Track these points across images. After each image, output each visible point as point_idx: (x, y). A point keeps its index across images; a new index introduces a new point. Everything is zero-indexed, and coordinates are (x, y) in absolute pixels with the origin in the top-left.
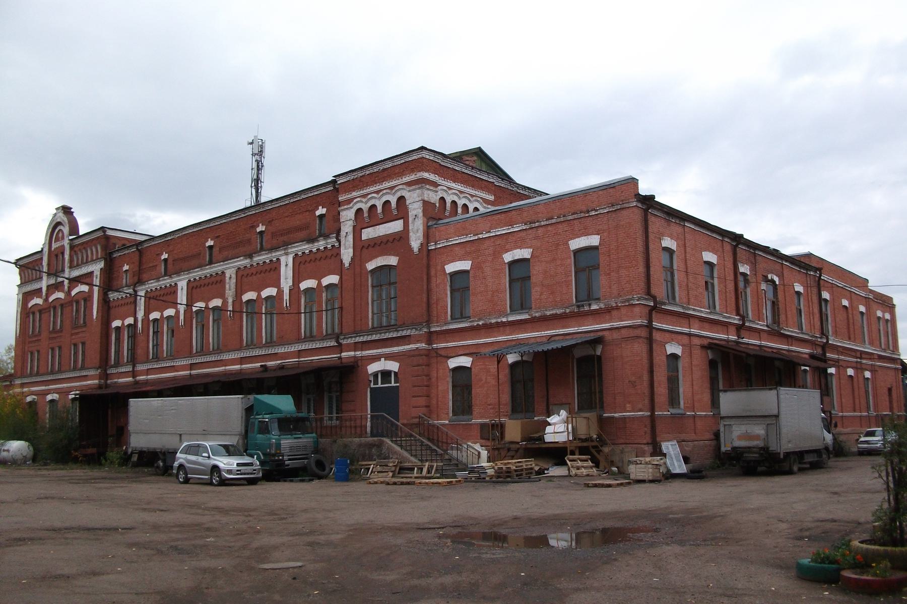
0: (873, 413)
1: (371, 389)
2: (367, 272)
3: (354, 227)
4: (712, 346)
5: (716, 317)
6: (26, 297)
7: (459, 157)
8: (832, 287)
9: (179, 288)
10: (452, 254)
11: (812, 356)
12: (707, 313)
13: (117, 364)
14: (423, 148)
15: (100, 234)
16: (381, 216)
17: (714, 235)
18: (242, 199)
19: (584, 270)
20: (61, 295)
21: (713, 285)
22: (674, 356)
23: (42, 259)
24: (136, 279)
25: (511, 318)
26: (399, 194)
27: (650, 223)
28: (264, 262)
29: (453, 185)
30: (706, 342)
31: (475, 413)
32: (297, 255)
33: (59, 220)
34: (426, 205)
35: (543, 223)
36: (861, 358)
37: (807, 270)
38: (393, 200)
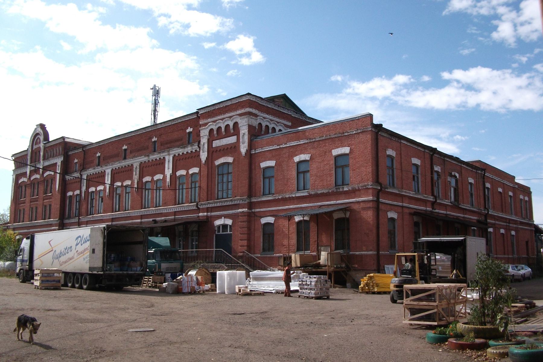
0: (516, 256)
1: (216, 235)
2: (215, 166)
3: (208, 140)
4: (416, 213)
5: (419, 197)
6: (17, 177)
7: (272, 99)
8: (492, 182)
9: (107, 173)
10: (266, 156)
11: (478, 221)
12: (413, 194)
13: (69, 217)
14: (249, 94)
15: (62, 140)
16: (224, 133)
17: (419, 148)
18: (146, 122)
19: (340, 167)
20: (38, 176)
21: (418, 178)
22: (392, 219)
23: (27, 155)
24: (82, 167)
25: (298, 195)
26: (234, 121)
27: (379, 141)
28: (156, 159)
29: (267, 116)
30: (412, 211)
31: (275, 250)
32: (175, 155)
33: (38, 132)
34: (250, 127)
35: (317, 139)
36: (509, 223)
37: (477, 170)
38: (231, 124)
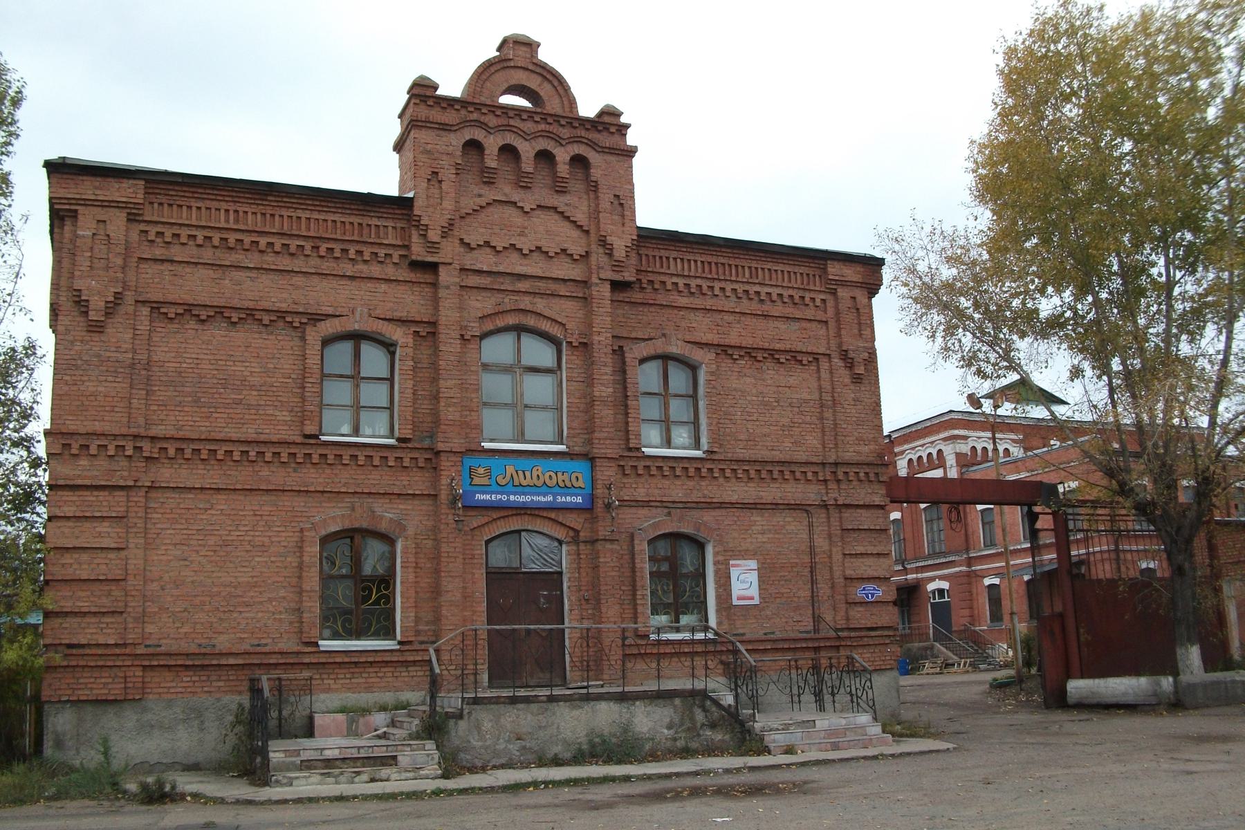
26: (938, 448)
34: (959, 456)
